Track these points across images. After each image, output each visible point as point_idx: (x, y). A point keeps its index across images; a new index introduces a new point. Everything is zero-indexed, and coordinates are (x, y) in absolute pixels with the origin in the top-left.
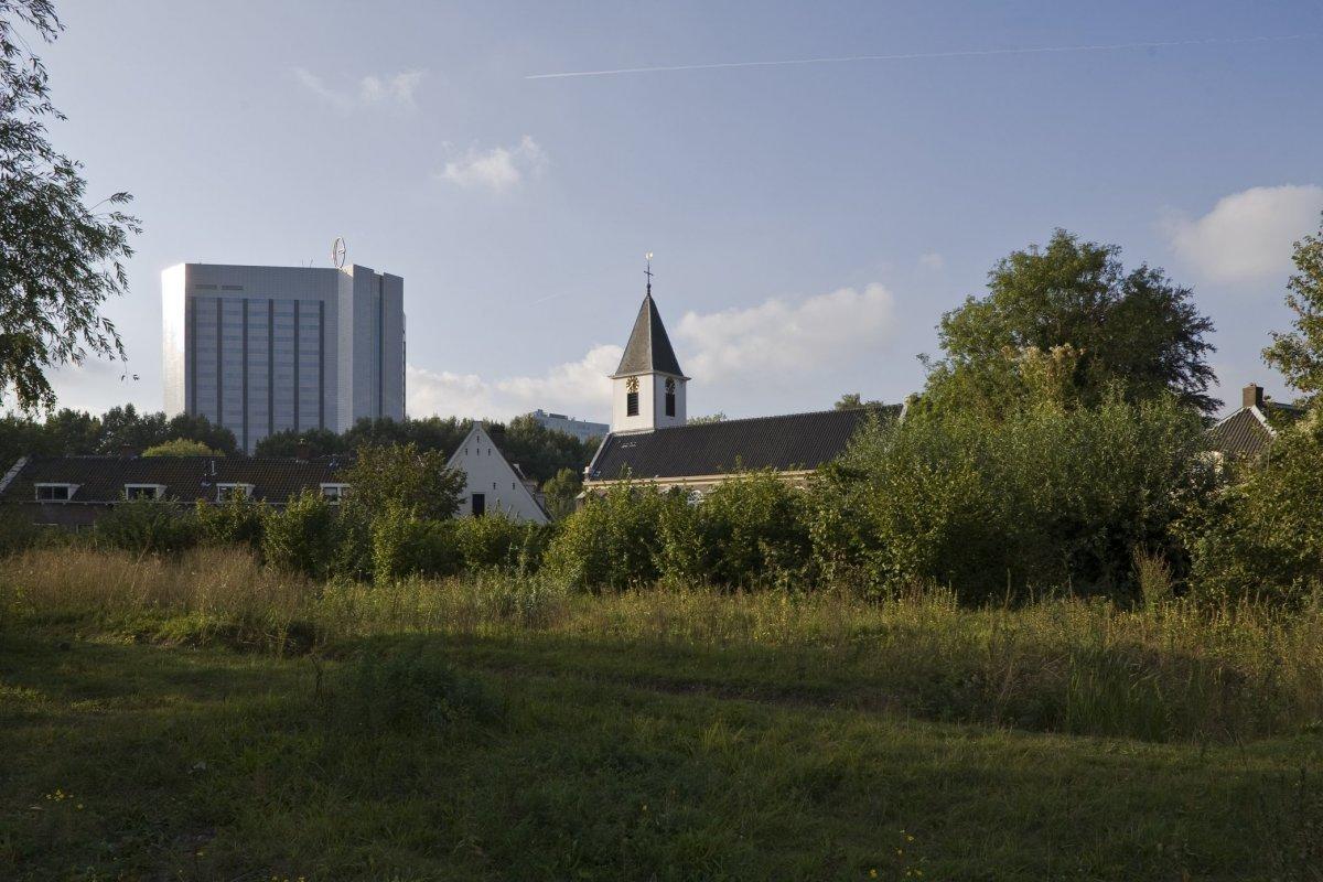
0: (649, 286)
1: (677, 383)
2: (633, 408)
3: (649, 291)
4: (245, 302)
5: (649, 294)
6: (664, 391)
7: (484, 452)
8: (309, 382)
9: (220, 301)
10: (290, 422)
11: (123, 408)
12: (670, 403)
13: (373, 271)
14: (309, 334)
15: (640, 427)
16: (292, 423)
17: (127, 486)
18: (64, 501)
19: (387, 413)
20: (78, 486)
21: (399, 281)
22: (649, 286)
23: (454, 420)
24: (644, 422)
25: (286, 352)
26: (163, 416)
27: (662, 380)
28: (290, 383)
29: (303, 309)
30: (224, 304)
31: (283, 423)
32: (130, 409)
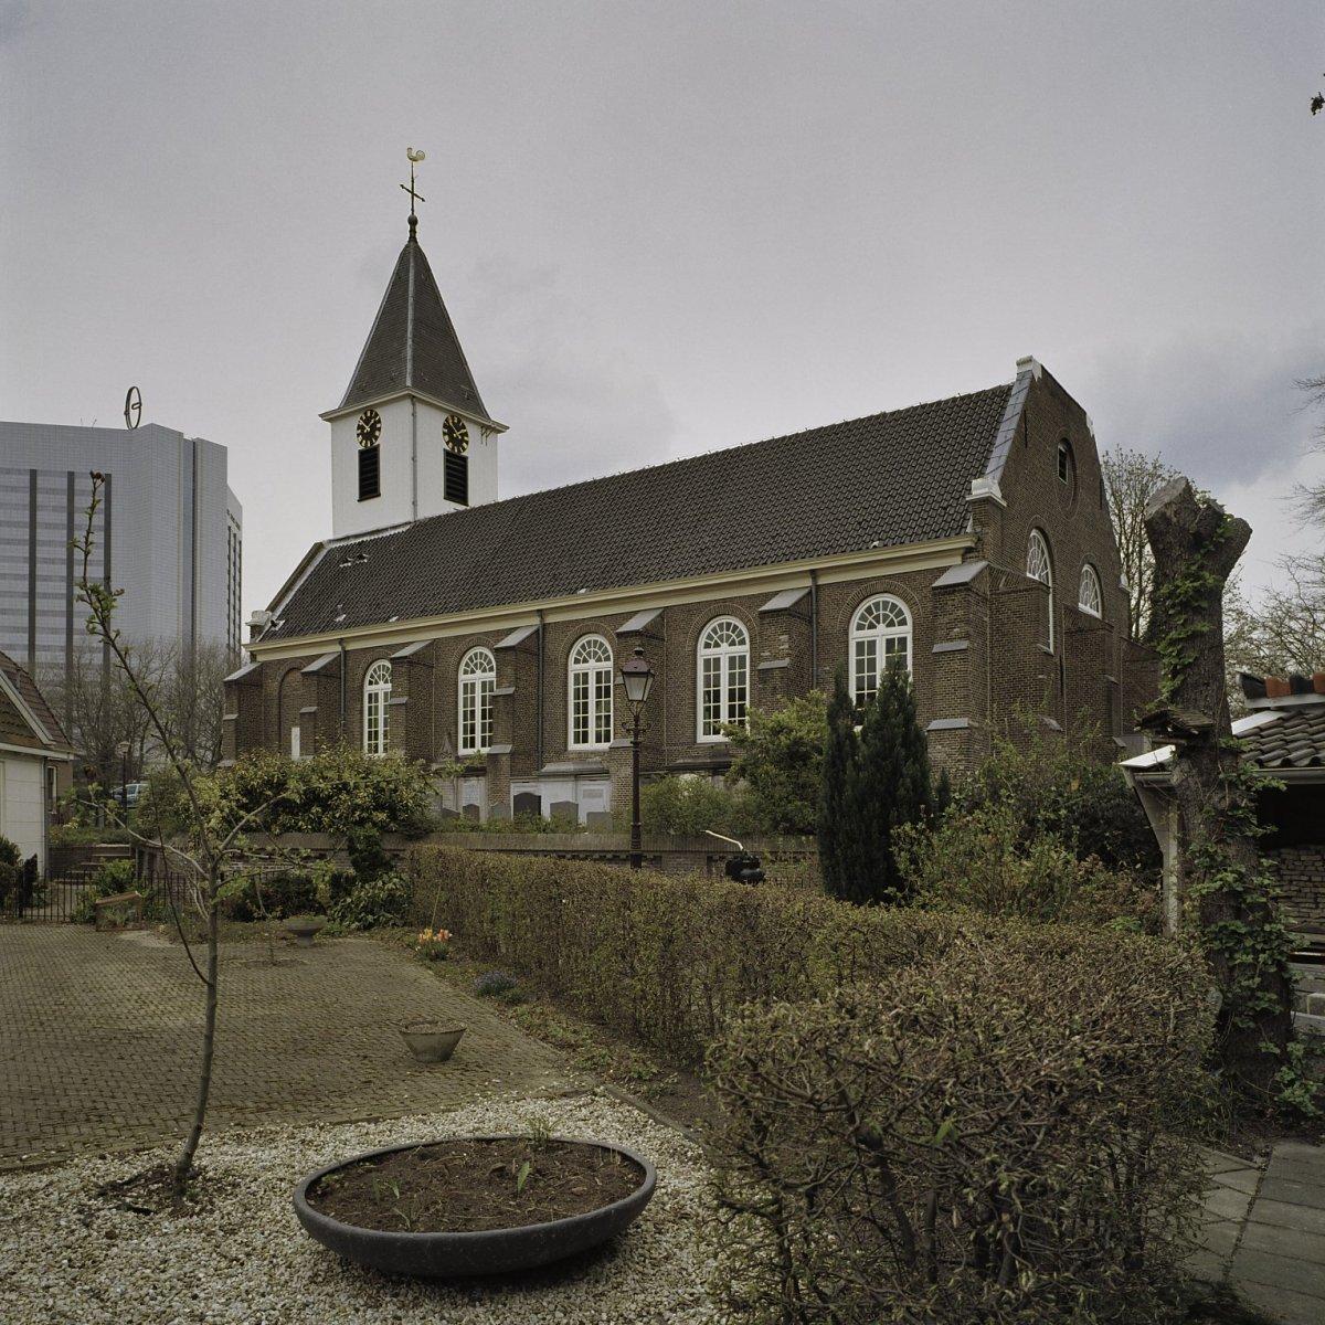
0: (413, 222)
1: (473, 432)
3: (413, 231)
22: (413, 222)
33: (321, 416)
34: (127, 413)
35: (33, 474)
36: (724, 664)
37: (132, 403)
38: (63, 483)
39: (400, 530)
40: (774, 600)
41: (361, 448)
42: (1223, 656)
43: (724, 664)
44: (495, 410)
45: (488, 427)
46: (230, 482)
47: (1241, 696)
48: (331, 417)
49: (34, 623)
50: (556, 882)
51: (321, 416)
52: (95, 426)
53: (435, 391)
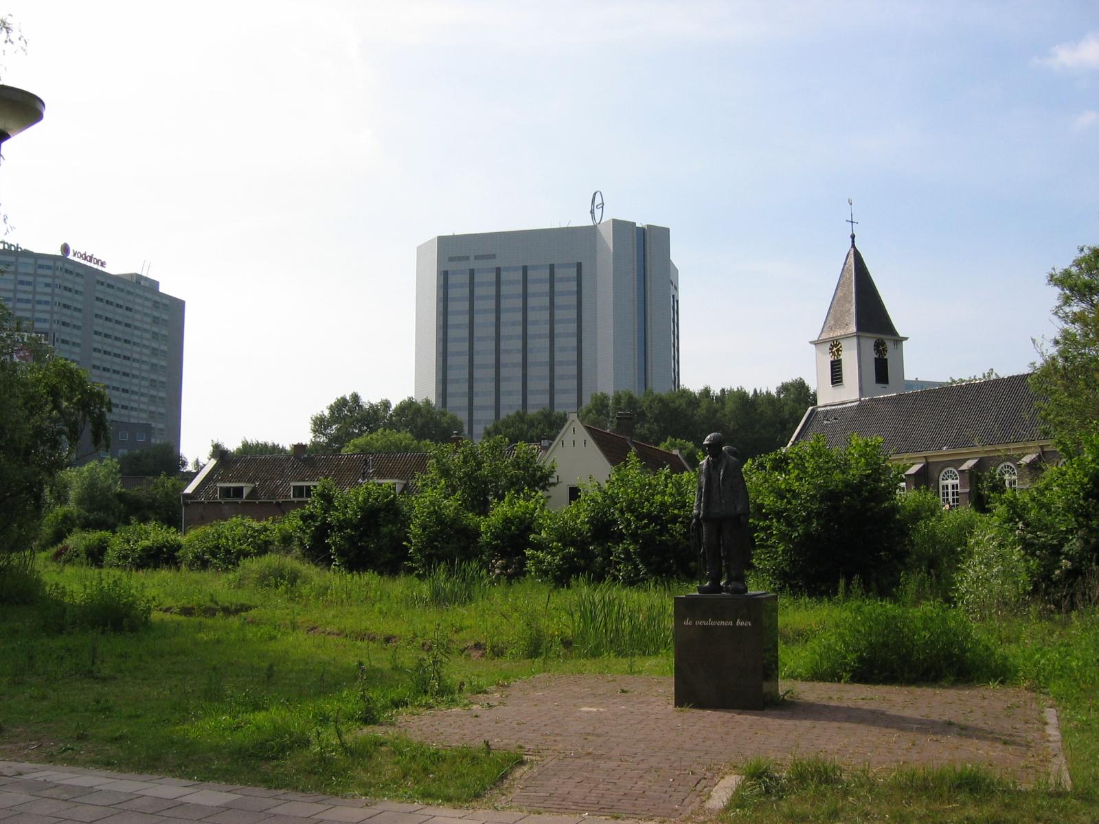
0: (853, 237)
1: (889, 345)
3: (853, 242)
4: (498, 270)
5: (853, 245)
6: (871, 355)
7: (580, 443)
8: (565, 355)
9: (472, 272)
10: (545, 400)
12: (882, 370)
13: (154, 285)
14: (566, 301)
15: (845, 399)
17: (293, 484)
18: (240, 501)
19: (660, 388)
20: (253, 485)
21: (664, 233)
22: (853, 237)
23: (386, 405)
24: (849, 392)
25: (513, 324)
26: (386, 405)
27: (869, 344)
28: (545, 357)
31: (511, 405)
32: (355, 398)
33: (810, 342)
34: (592, 212)
35: (525, 269)
36: (950, 487)
37: (596, 204)
38: (546, 274)
39: (853, 404)
41: (832, 359)
43: (950, 487)
44: (901, 330)
45: (897, 341)
46: (672, 258)
47: (312, 747)
48: (817, 343)
49: (496, 371)
50: (31, 697)
51: (810, 342)
52: (570, 226)
53: (869, 331)
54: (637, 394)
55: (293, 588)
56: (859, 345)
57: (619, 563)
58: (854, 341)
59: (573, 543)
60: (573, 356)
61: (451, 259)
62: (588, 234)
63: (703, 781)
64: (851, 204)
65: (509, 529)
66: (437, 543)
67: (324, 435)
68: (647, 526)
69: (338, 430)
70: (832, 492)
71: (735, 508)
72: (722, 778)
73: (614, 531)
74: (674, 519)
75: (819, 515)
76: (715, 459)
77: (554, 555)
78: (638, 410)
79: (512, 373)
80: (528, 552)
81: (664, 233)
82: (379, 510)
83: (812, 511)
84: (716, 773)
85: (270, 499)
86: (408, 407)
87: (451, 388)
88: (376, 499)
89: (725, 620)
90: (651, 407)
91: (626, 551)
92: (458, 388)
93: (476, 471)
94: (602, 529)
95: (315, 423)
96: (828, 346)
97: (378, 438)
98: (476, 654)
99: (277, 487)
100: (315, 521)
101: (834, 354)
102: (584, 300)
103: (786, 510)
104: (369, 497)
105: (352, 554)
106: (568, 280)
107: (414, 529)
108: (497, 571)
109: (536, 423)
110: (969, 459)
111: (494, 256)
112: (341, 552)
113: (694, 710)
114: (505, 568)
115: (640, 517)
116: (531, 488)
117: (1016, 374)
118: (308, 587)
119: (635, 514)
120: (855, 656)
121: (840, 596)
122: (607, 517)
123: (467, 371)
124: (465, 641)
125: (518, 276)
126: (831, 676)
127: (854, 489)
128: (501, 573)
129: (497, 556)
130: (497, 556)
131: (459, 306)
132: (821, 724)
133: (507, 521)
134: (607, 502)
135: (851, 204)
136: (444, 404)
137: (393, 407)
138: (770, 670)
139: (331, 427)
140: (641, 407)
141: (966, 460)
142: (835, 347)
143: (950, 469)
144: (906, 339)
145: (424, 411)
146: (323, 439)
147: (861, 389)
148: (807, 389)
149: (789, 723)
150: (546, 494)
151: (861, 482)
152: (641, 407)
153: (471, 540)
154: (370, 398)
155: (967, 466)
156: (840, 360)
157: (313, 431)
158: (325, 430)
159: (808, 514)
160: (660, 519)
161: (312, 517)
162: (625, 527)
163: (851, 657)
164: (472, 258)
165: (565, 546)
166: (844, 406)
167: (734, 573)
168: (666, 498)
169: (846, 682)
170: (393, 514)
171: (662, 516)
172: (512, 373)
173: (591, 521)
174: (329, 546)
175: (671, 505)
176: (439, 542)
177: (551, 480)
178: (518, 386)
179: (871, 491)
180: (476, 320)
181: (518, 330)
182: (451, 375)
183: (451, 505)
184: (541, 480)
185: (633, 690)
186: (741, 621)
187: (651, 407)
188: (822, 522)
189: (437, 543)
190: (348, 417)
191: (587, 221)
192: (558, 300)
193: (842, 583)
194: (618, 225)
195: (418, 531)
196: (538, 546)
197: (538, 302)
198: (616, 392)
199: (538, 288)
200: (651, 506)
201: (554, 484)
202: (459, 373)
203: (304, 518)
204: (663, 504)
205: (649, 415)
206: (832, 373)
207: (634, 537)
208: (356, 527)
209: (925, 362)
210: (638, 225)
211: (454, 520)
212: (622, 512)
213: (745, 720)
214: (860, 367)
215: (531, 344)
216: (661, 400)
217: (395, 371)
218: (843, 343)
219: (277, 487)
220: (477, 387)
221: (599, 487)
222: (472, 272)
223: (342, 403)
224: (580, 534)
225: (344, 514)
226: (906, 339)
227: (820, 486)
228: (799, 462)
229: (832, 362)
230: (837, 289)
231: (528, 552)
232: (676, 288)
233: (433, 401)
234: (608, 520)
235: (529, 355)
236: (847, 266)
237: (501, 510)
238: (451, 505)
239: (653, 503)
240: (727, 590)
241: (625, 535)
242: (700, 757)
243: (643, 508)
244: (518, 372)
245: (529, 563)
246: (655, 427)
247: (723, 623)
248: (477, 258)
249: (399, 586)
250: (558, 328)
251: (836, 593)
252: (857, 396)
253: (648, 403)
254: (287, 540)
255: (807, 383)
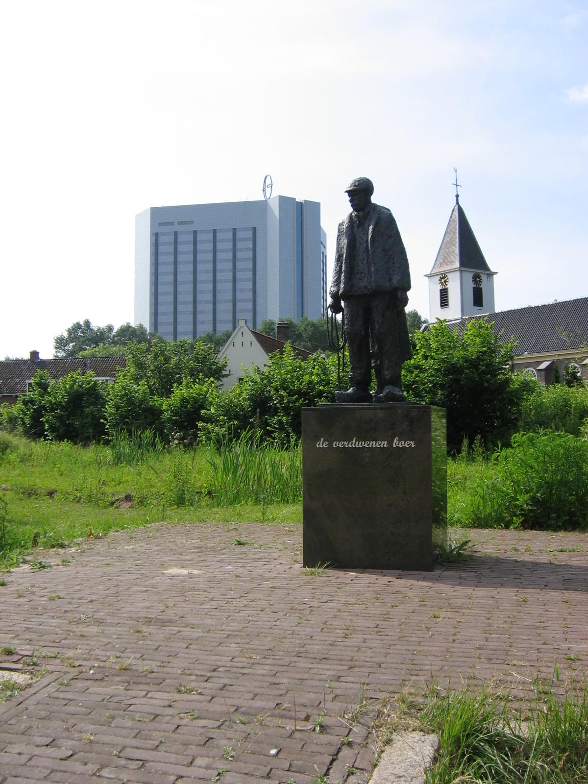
0: (457, 196)
1: (484, 278)
2: (444, 302)
3: (457, 200)
4: (195, 232)
5: (457, 203)
6: (470, 285)
8: (244, 295)
9: (176, 234)
11: (82, 323)
12: (478, 298)
16: (211, 329)
22: (457, 196)
23: (110, 328)
24: (453, 313)
26: (110, 328)
27: (469, 276)
29: (240, 235)
30: (237, 233)
32: (87, 323)
34: (264, 190)
35: (215, 231)
37: (267, 184)
40: (542, 364)
41: (441, 288)
42: (431, 464)
44: (492, 267)
45: (490, 274)
48: (429, 276)
49: (174, 328)
51: (425, 275)
54: (296, 321)
55: (4, 457)
56: (461, 277)
57: (274, 432)
58: (458, 274)
59: (237, 417)
60: (250, 295)
61: (160, 224)
62: (261, 207)
63: (345, 751)
64: (456, 171)
65: (186, 407)
66: (127, 420)
67: (64, 350)
68: (297, 400)
69: (74, 346)
70: (454, 366)
71: (390, 280)
72: (388, 742)
73: (270, 407)
74: (320, 395)
75: (442, 387)
76: (361, 213)
77: (221, 426)
78: (296, 332)
79: (205, 308)
80: (200, 424)
81: (316, 207)
82: (82, 395)
83: (437, 383)
84: (376, 729)
85: (10, 393)
86: (128, 334)
87: (161, 319)
88: (81, 386)
89: (375, 440)
90: (306, 330)
91: (280, 422)
92: (166, 319)
93: (164, 364)
94: (261, 404)
95: (57, 342)
96: (438, 278)
97: (100, 351)
98: (126, 505)
99: (16, 384)
100: (34, 405)
101: (442, 283)
102: (257, 254)
103: (415, 382)
104: (74, 384)
105: (61, 431)
106: (246, 240)
107: (109, 409)
108: (176, 442)
109: (221, 342)
110: (544, 361)
111: (192, 222)
112: (53, 429)
113: (331, 572)
114: (182, 439)
115: (291, 394)
116: (206, 376)
117: (579, 298)
118: (15, 455)
119: (288, 391)
120: (527, 497)
121: (464, 454)
122: (264, 395)
123: (172, 307)
124: (118, 493)
125: (210, 236)
126: (499, 521)
127: (474, 364)
128: (179, 443)
129: (176, 429)
130: (176, 429)
131: (166, 259)
132: (532, 594)
133: (184, 400)
134: (264, 382)
135: (456, 171)
136: (156, 329)
137: (115, 330)
138: (436, 513)
139: (69, 345)
140: (298, 330)
141: (542, 362)
142: (443, 279)
143: (531, 369)
144: (496, 273)
145: (138, 333)
146: (61, 354)
147: (462, 310)
148: (420, 318)
149: (481, 594)
150: (219, 383)
151: (478, 358)
152: (298, 330)
153: (156, 417)
154: (98, 323)
155: (543, 366)
156: (447, 289)
157: (56, 348)
158: (64, 346)
159: (434, 386)
160: (308, 395)
161: (32, 401)
162: (279, 402)
163: (522, 499)
164: (176, 224)
165: (230, 419)
166: (450, 323)
167: (387, 374)
168: (313, 377)
169: (516, 528)
170: (94, 398)
171: (309, 392)
172: (205, 308)
173: (251, 398)
174: (43, 424)
175: (317, 383)
176: (129, 419)
177: (224, 373)
178: (210, 317)
179: (487, 366)
180: (179, 270)
181: (210, 277)
182: (161, 309)
183: (140, 389)
184: (217, 373)
185: (253, 541)
186: (399, 441)
187: (306, 330)
188: (446, 392)
189: (127, 420)
190: (82, 336)
191: (263, 199)
192: (239, 255)
193: (466, 442)
194: (283, 200)
195: (113, 411)
196: (208, 420)
197: (225, 256)
198: (281, 319)
199: (225, 245)
200: (301, 384)
201: (226, 376)
202: (166, 308)
203: (25, 403)
204: (310, 382)
205: (304, 335)
206: (441, 301)
207: (286, 410)
208: (63, 408)
209: (507, 296)
210: (297, 200)
211: (142, 401)
212: (277, 390)
213: (411, 589)
214: (462, 293)
215: (219, 286)
216: (313, 325)
217: (119, 302)
218: (450, 276)
219: (16, 384)
220: (180, 318)
221: (258, 371)
222: (176, 234)
223: (77, 326)
224: (243, 409)
225: (55, 398)
226: (496, 273)
227: (443, 361)
228: (425, 343)
229: (441, 290)
230: (445, 235)
231: (200, 424)
232: (325, 247)
233: (147, 326)
234: (266, 397)
235: (218, 295)
236: (453, 218)
237: (179, 392)
238: (139, 390)
239: (303, 382)
240: (379, 400)
241: (279, 408)
242: (338, 679)
243: (294, 387)
244: (210, 307)
245: (200, 433)
246: (309, 344)
247: (373, 444)
248: (180, 223)
249: (90, 453)
250: (239, 275)
251: (459, 452)
252: (459, 316)
253: (304, 326)
254: (12, 420)
255: (419, 313)
